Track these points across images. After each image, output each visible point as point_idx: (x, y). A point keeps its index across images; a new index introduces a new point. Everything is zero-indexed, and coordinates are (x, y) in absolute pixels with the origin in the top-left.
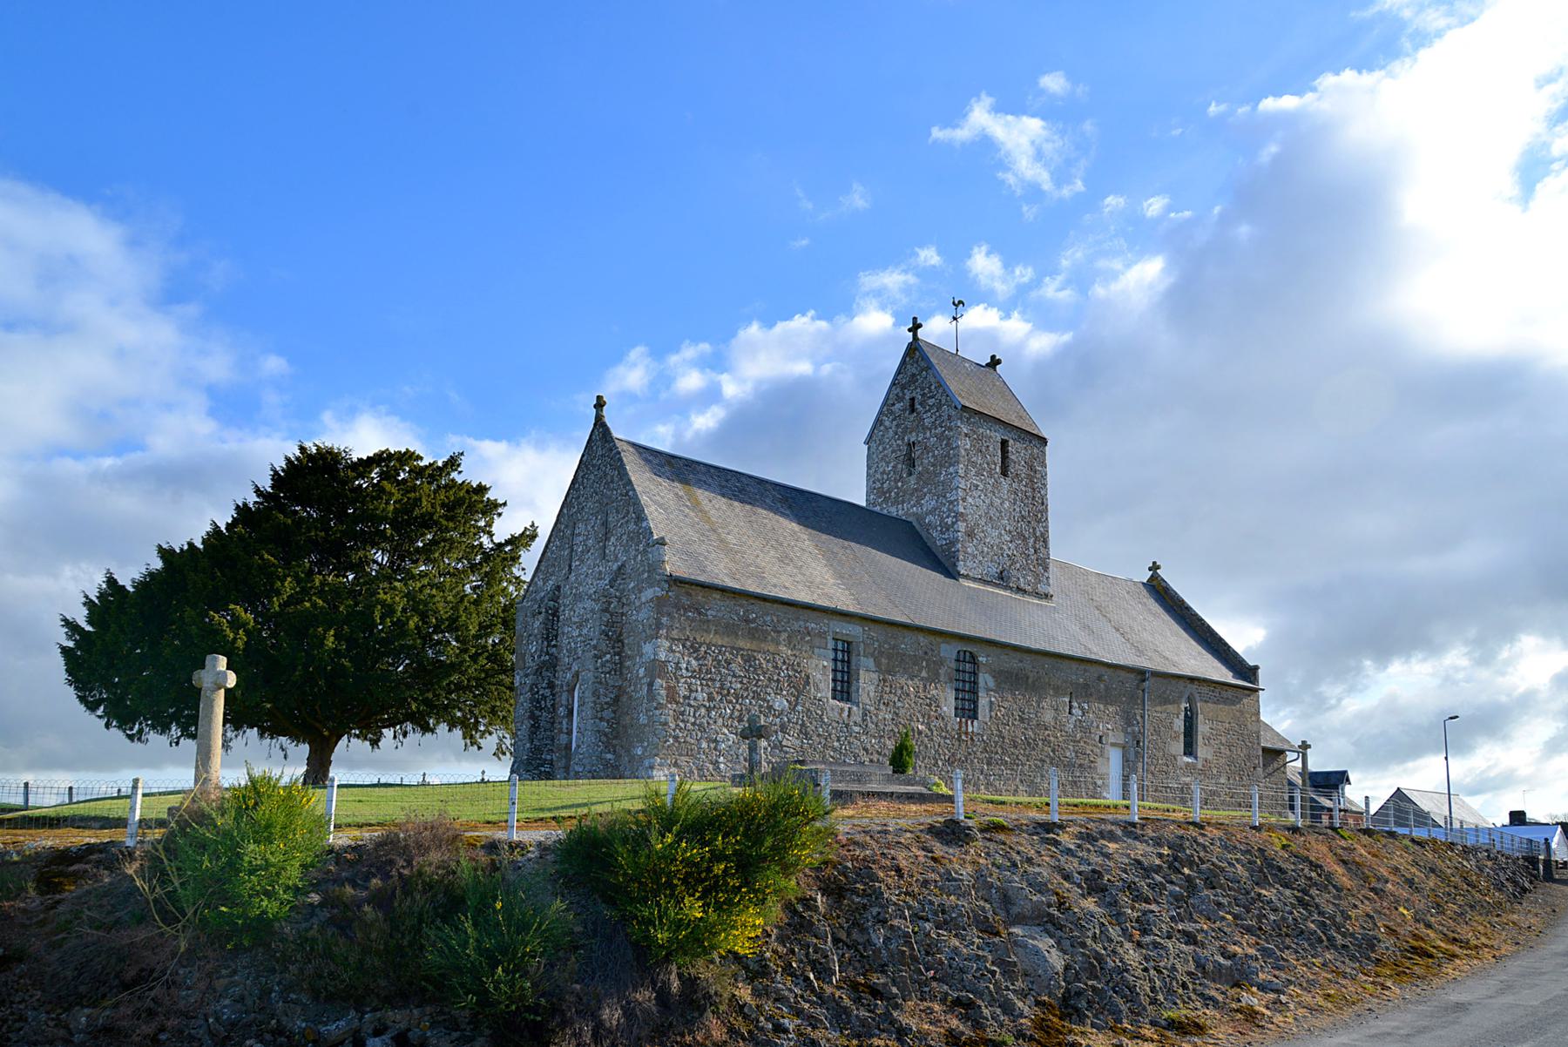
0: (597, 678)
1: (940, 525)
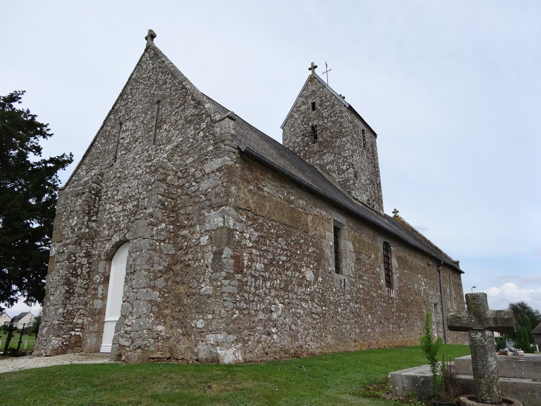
0: (151, 245)
1: (338, 170)
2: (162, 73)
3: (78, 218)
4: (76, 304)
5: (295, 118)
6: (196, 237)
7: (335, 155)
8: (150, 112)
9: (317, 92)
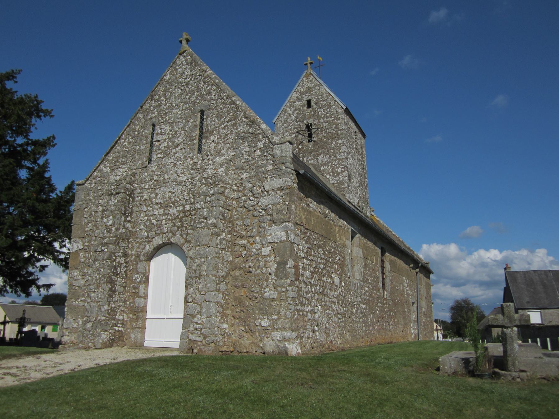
1: (332, 172)
2: (205, 82)
3: (114, 217)
4: (117, 301)
5: (289, 114)
6: (256, 248)
7: (330, 157)
8: (192, 120)
9: (313, 89)
